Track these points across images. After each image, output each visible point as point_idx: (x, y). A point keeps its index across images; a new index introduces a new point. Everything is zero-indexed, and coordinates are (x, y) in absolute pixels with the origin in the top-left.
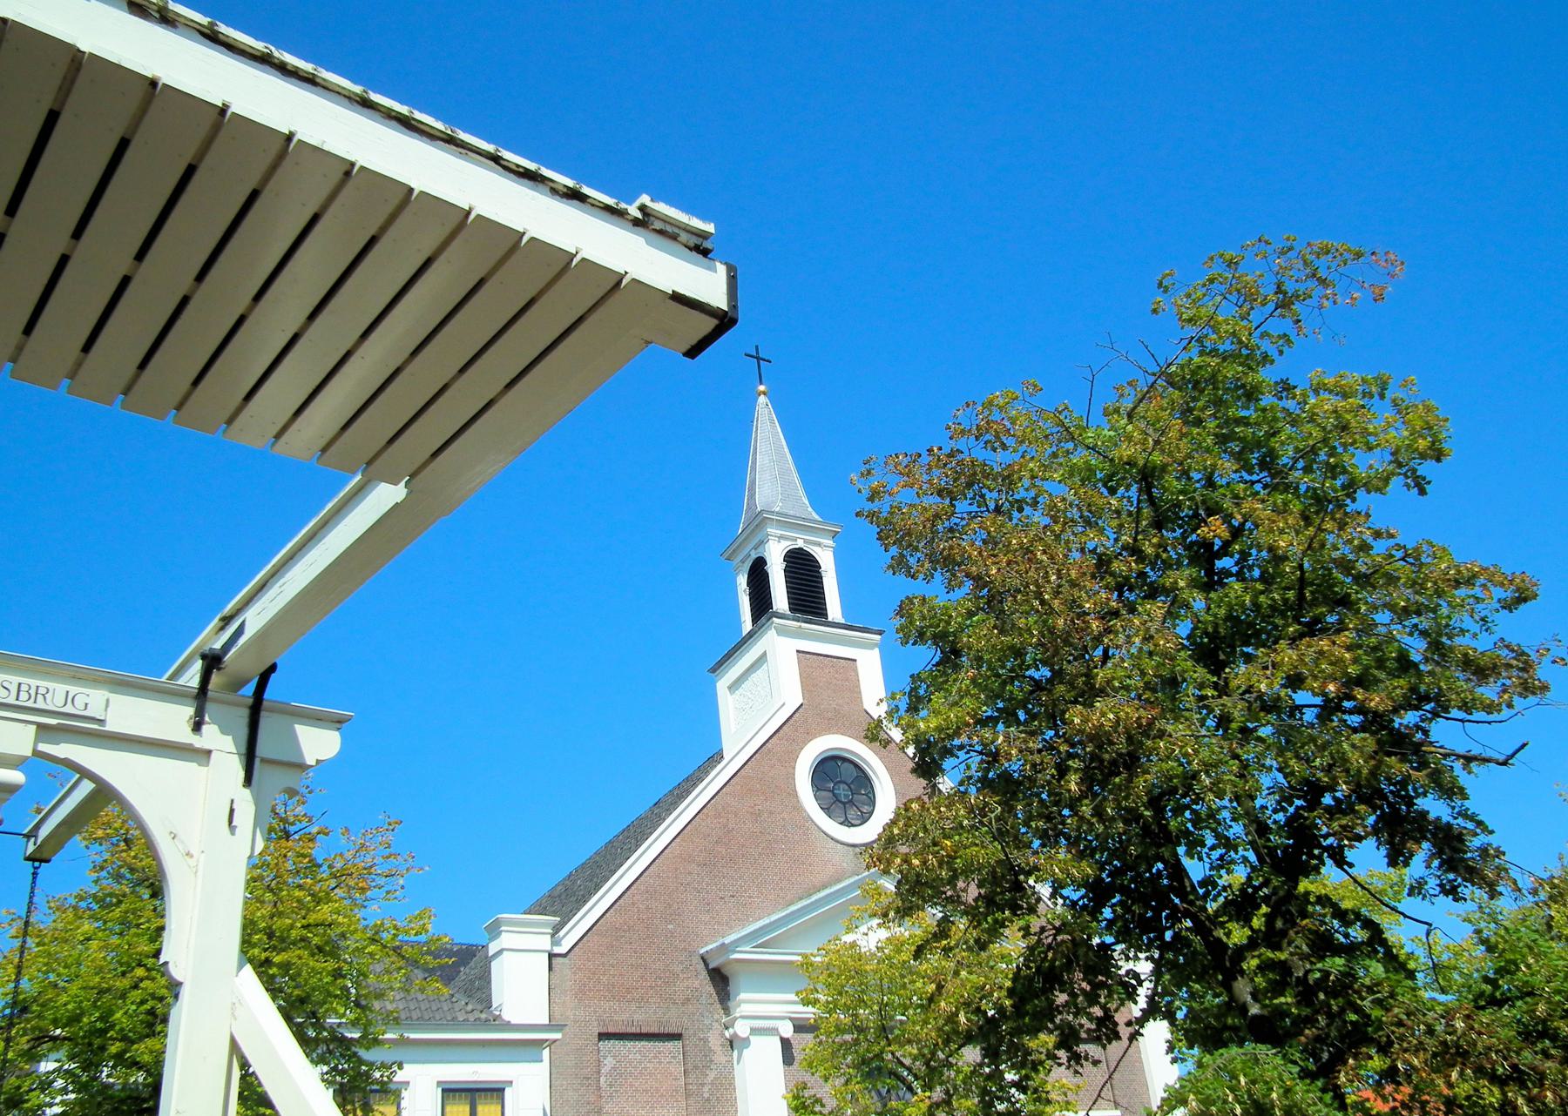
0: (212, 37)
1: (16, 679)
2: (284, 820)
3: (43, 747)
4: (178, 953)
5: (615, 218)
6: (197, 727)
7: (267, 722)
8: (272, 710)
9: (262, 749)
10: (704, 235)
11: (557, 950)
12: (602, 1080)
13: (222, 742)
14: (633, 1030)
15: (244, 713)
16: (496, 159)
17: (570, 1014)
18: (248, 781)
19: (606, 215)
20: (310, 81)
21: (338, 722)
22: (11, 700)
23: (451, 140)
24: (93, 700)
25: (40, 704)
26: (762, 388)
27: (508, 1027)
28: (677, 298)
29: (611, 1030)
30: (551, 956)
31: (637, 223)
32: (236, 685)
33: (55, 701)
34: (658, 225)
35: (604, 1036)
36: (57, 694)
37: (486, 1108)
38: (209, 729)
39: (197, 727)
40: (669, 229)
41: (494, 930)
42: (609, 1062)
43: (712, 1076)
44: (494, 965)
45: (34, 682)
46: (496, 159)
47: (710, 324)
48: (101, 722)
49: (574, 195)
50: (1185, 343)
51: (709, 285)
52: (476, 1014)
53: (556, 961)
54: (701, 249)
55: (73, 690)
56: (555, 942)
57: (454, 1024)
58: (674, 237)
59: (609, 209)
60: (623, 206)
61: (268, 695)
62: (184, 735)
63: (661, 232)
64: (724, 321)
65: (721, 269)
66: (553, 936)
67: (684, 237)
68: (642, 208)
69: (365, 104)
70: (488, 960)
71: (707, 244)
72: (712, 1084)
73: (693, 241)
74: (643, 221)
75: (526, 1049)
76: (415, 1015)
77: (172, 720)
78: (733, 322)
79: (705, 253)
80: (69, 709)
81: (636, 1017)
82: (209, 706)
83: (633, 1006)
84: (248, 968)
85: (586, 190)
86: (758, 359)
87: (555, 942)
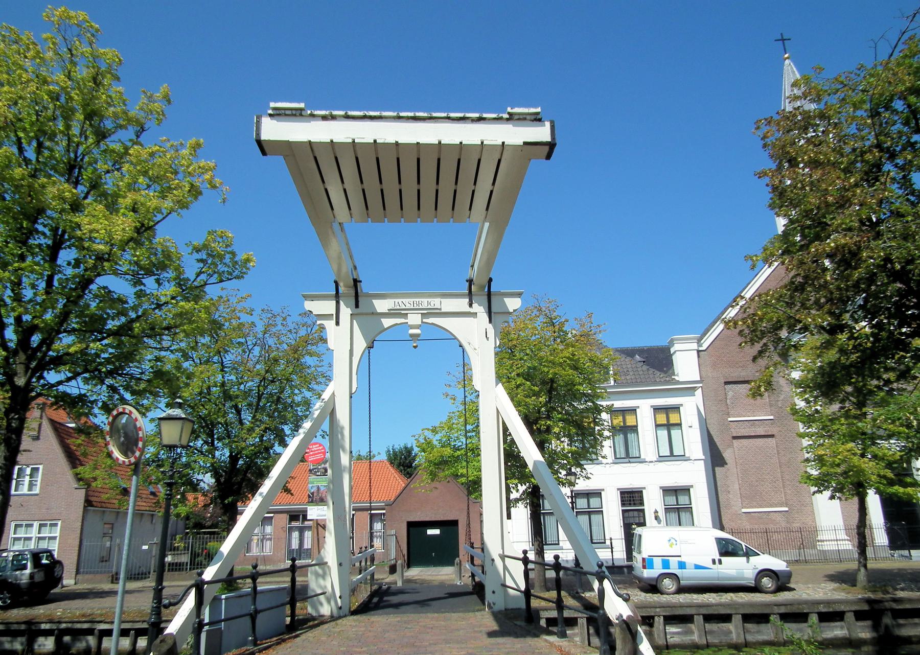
0: (347, 117)
1: (412, 300)
2: (551, 318)
3: (424, 320)
4: (477, 383)
5: (499, 121)
6: (471, 305)
7: (493, 299)
8: (495, 295)
9: (494, 309)
10: (538, 114)
11: (701, 349)
12: (728, 401)
13: (479, 309)
14: (741, 380)
15: (486, 297)
16: (448, 118)
17: (710, 374)
18: (490, 321)
19: (496, 121)
20: (380, 118)
21: (519, 295)
22: (412, 307)
23: (431, 118)
24: (436, 302)
25: (421, 307)
26: (786, 56)
27: (678, 382)
28: (525, 143)
29: (730, 380)
30: (698, 351)
31: (507, 119)
32: (482, 288)
33: (425, 306)
34: (516, 117)
35: (727, 383)
36: (425, 302)
37: (673, 415)
38: (475, 305)
39: (471, 305)
40: (521, 117)
41: (672, 343)
42: (730, 394)
43: (782, 397)
44: (674, 357)
45: (417, 300)
46: (448, 118)
47: (547, 148)
48: (440, 309)
49: (481, 119)
50: (911, 18)
51: (542, 133)
52: (664, 378)
53: (701, 353)
54: (537, 119)
55: (430, 300)
56: (700, 345)
57: (655, 383)
58: (525, 119)
59: (495, 119)
60: (501, 115)
61: (492, 290)
62: (467, 309)
63: (519, 119)
64: (551, 146)
65: (548, 124)
66: (698, 343)
67: (528, 117)
68: (509, 113)
69: (399, 118)
70: (671, 355)
71: (539, 117)
72: (782, 400)
73: (533, 117)
74: (511, 118)
75: (689, 391)
76: (634, 381)
77: (461, 304)
78: (555, 144)
79: (540, 120)
80: (429, 307)
81: (742, 374)
82: (474, 297)
83: (740, 369)
84: (500, 385)
85: (485, 116)
86: (783, 40)
87: (700, 345)
